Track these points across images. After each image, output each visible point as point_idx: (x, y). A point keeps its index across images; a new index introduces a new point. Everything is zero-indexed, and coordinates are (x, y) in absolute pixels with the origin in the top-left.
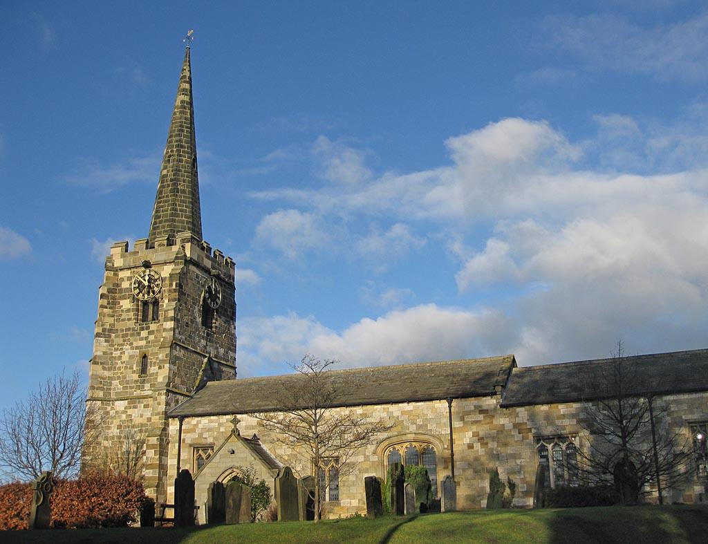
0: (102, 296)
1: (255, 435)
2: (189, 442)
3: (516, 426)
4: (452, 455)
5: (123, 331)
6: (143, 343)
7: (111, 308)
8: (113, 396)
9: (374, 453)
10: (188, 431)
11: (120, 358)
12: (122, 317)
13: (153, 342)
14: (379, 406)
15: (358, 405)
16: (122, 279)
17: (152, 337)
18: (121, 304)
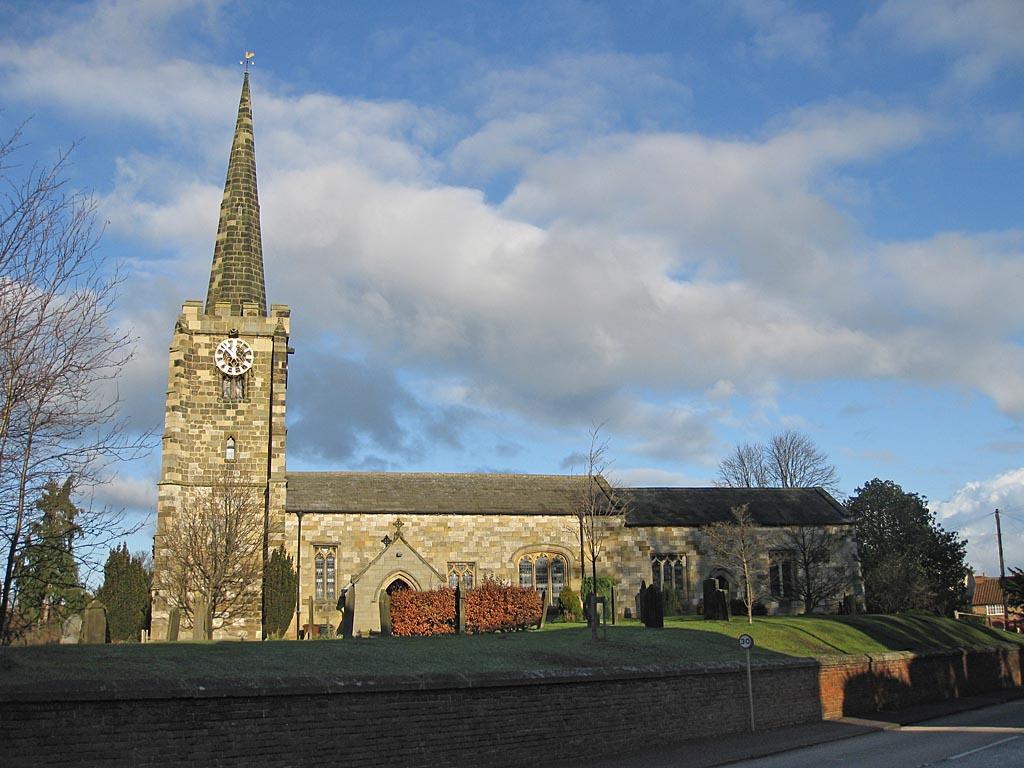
0: (177, 363)
1: (387, 537)
2: (310, 539)
3: (638, 543)
4: (583, 566)
6: (230, 423)
7: (187, 378)
9: (511, 560)
11: (199, 437)
14: (515, 517)
15: (495, 514)
16: (198, 345)
17: (241, 418)
18: (198, 374)
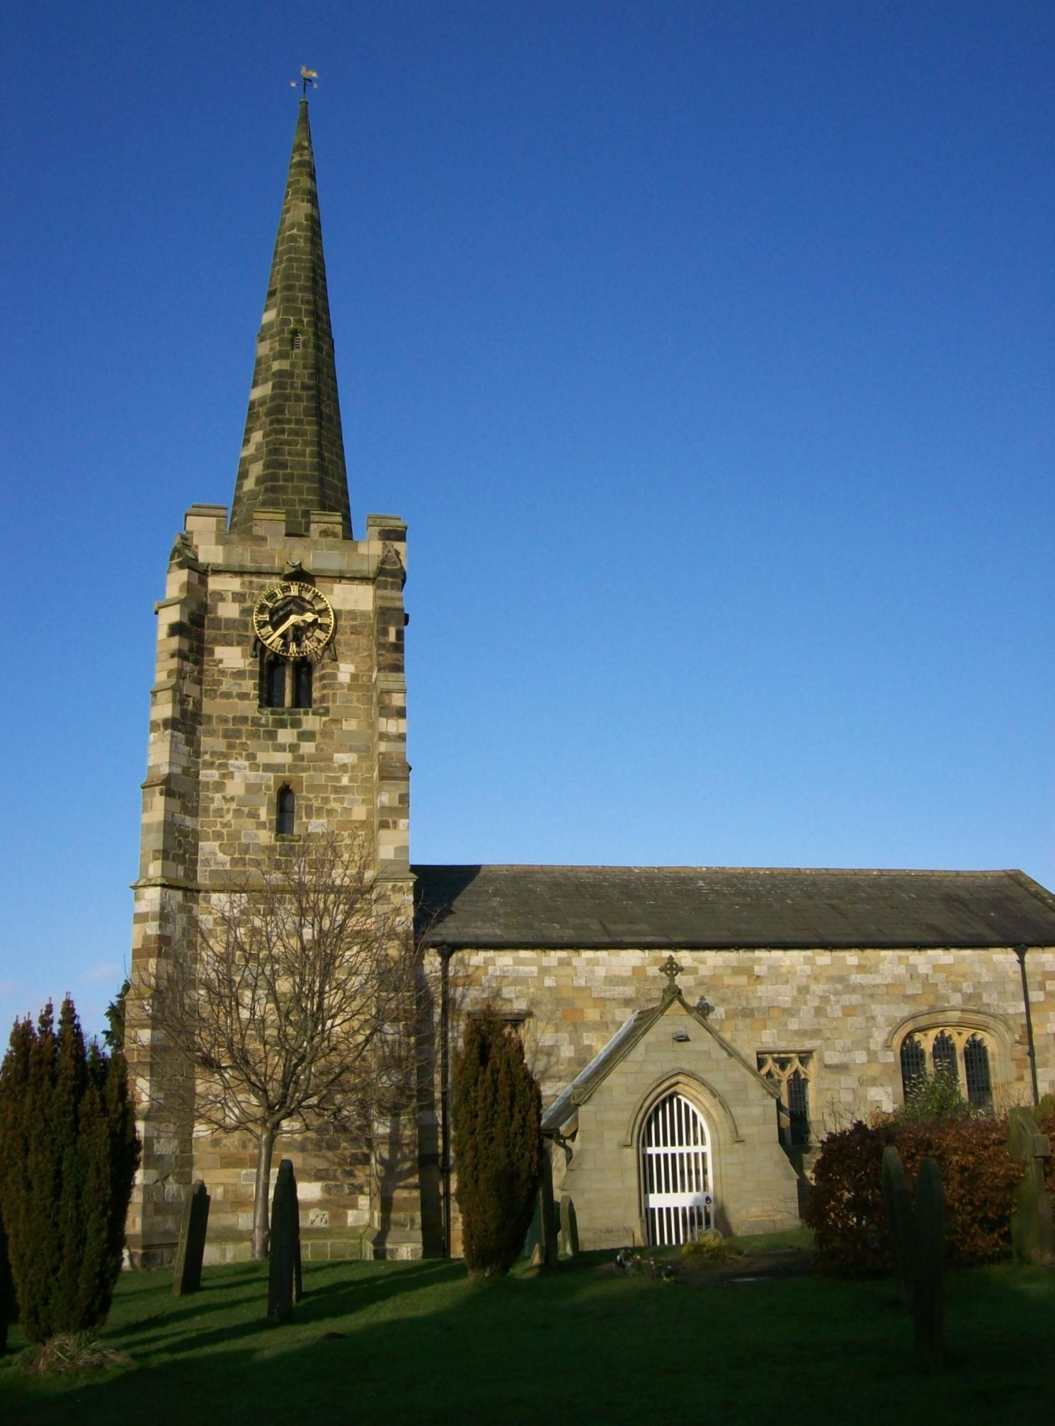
6: (285, 758)
8: (202, 879)
11: (220, 786)
12: (224, 688)
13: (312, 759)
16: (220, 596)
17: (308, 748)
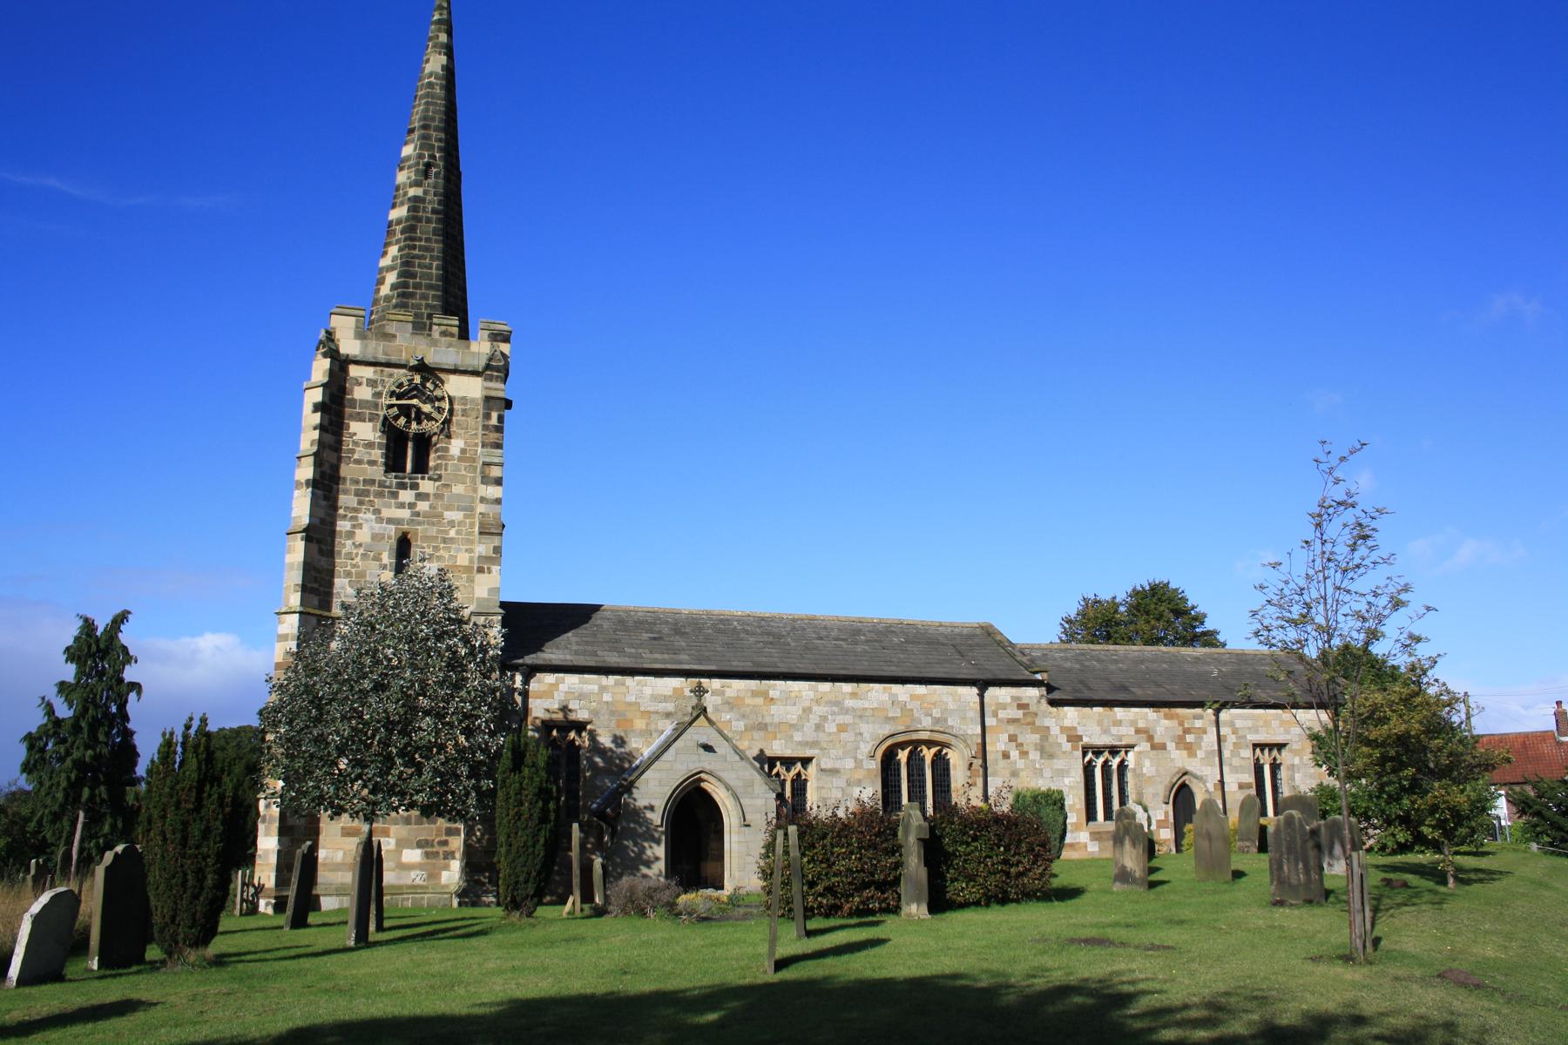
5: (357, 482)
6: (405, 514)
10: (540, 696)
17: (423, 506)
